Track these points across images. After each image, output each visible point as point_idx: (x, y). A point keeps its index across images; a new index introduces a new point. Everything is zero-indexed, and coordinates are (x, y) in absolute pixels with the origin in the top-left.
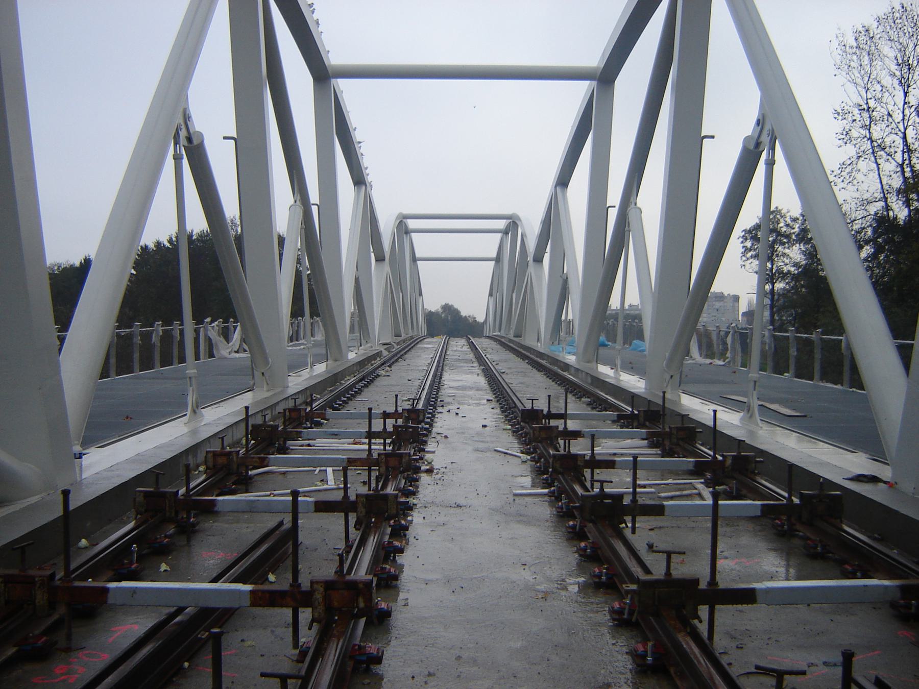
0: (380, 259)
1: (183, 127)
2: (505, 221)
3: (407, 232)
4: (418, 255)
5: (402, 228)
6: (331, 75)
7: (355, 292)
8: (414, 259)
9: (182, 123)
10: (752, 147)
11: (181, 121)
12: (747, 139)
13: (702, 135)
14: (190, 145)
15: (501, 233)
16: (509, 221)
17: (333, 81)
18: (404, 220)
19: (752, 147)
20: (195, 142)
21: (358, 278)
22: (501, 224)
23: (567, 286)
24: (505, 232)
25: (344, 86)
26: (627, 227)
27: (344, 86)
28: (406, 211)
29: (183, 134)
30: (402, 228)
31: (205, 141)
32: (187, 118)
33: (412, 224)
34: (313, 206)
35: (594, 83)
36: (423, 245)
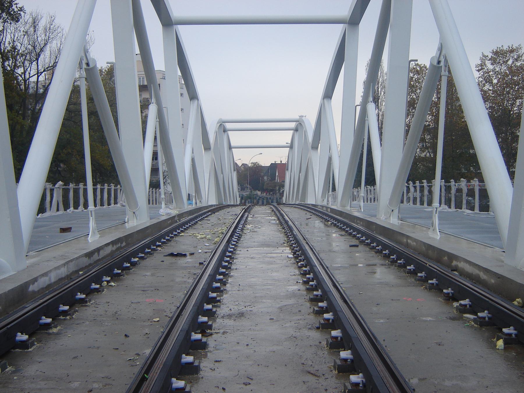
0: (207, 148)
1: (84, 58)
2: (295, 123)
3: (225, 131)
4: (233, 144)
5: (222, 129)
6: (174, 24)
7: (192, 171)
8: (230, 148)
9: (84, 55)
10: (436, 64)
11: (83, 55)
12: (432, 58)
13: (409, 60)
14: (88, 68)
15: (293, 130)
16: (298, 123)
17: (175, 26)
18: (223, 123)
19: (435, 63)
20: (91, 65)
21: (194, 158)
22: (293, 125)
23: (331, 162)
24: (296, 130)
25: (182, 30)
26: (366, 118)
27: (182, 30)
28: (225, 118)
29: (84, 62)
30: (222, 129)
31: (97, 65)
32: (86, 52)
33: (228, 126)
34: (164, 108)
35: (346, 25)
36: (236, 138)
